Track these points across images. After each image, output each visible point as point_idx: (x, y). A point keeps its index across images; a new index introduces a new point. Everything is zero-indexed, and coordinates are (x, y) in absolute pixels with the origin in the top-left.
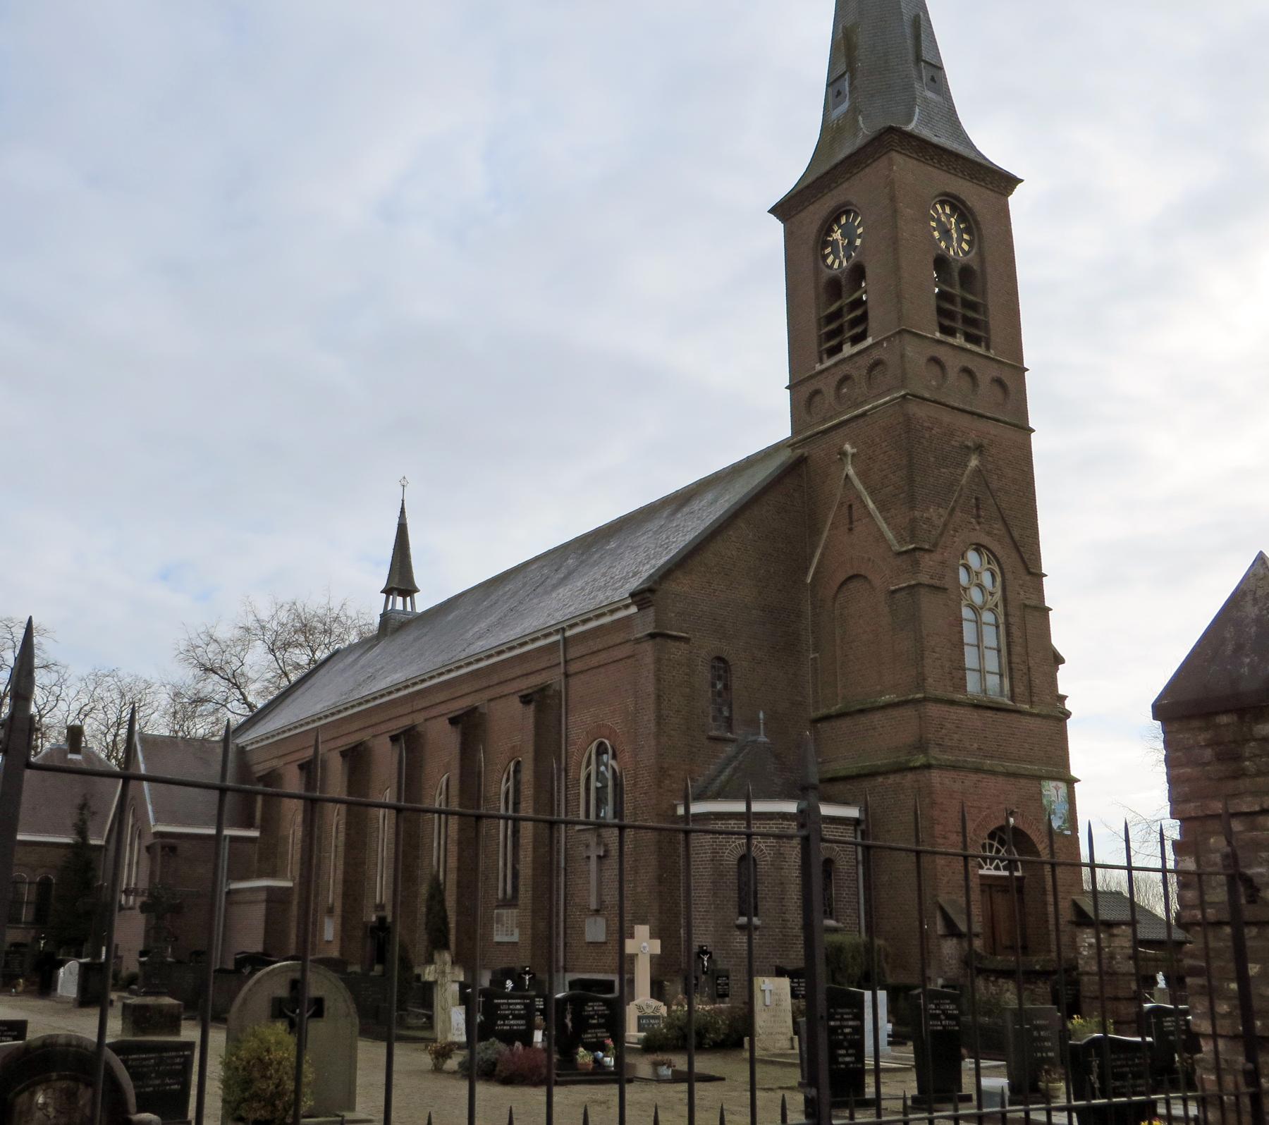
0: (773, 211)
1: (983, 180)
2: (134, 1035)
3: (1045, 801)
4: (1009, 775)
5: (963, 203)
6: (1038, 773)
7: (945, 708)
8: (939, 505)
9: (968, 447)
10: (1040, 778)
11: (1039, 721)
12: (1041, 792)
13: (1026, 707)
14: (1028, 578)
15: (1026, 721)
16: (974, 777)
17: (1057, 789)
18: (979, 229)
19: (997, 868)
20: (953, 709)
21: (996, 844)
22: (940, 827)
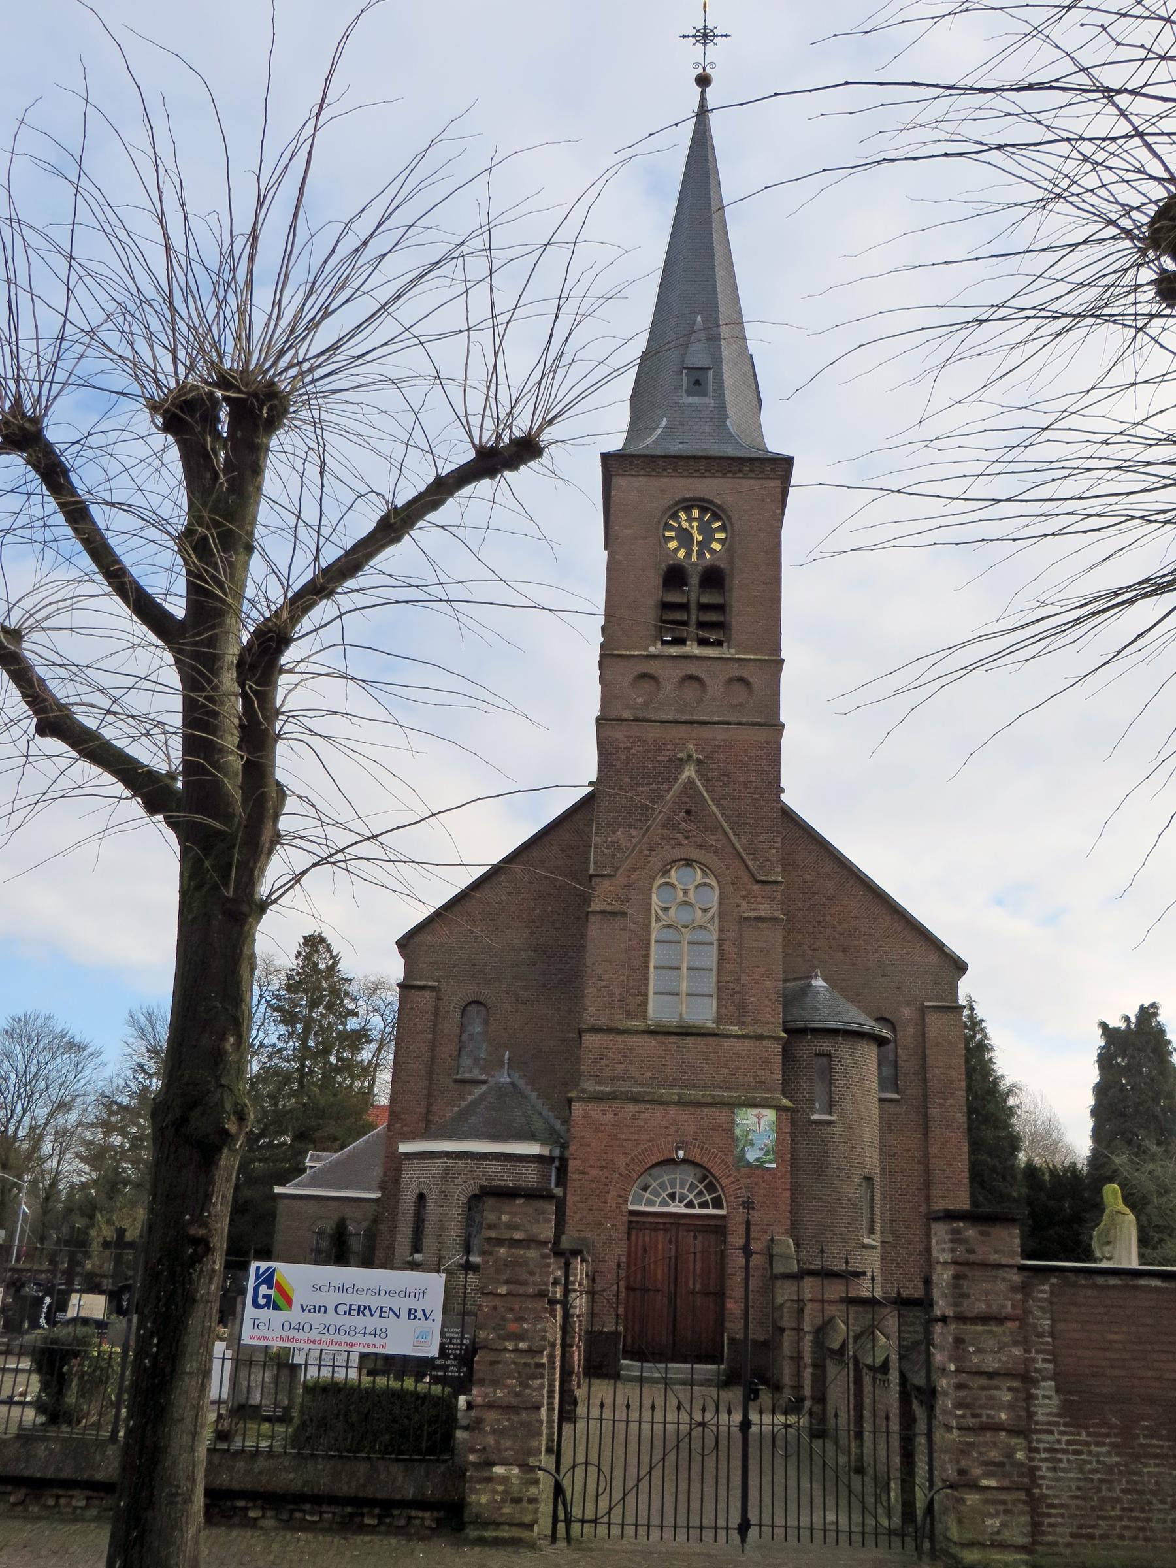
0: (1147, 1014)
1: (740, 471)
2: (1023, 1259)
3: (738, 1131)
4: (681, 1103)
5: (711, 502)
6: (731, 1101)
7: (608, 1038)
8: (631, 826)
9: (681, 760)
10: (732, 1105)
11: (748, 1043)
12: (733, 1122)
13: (735, 1029)
14: (756, 887)
15: (726, 1044)
16: (633, 1108)
17: (759, 1117)
18: (723, 510)
19: (690, 1205)
20: (620, 1038)
21: (701, 1187)
22: (577, 1162)
